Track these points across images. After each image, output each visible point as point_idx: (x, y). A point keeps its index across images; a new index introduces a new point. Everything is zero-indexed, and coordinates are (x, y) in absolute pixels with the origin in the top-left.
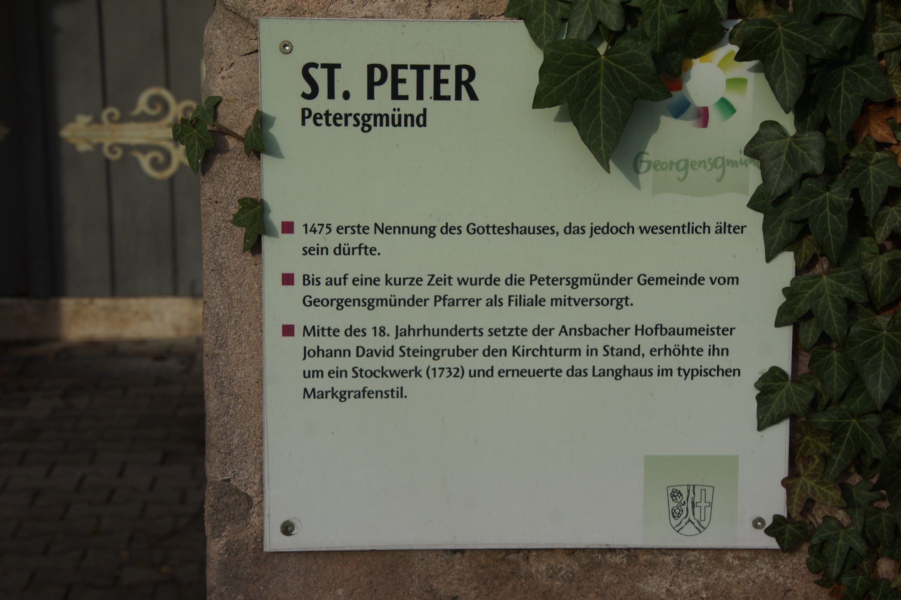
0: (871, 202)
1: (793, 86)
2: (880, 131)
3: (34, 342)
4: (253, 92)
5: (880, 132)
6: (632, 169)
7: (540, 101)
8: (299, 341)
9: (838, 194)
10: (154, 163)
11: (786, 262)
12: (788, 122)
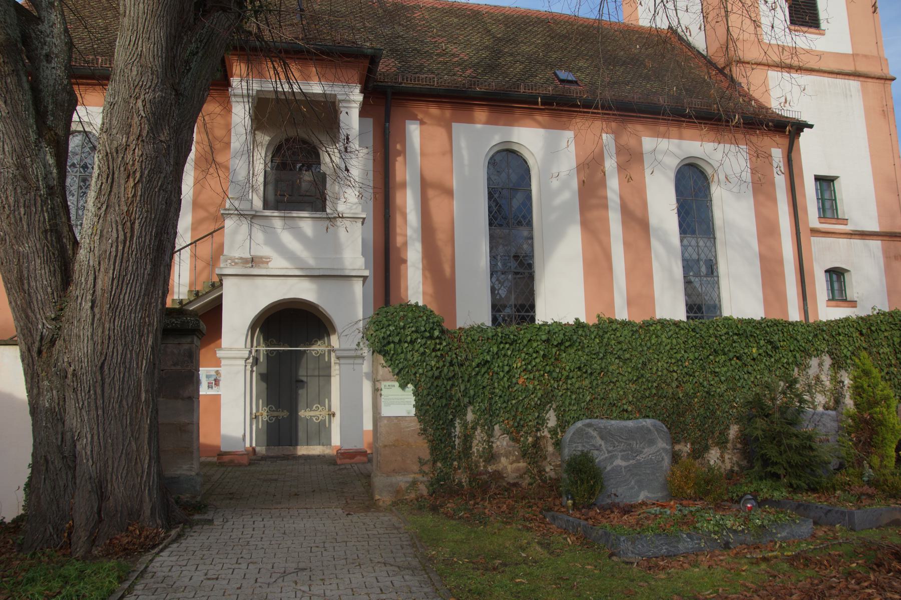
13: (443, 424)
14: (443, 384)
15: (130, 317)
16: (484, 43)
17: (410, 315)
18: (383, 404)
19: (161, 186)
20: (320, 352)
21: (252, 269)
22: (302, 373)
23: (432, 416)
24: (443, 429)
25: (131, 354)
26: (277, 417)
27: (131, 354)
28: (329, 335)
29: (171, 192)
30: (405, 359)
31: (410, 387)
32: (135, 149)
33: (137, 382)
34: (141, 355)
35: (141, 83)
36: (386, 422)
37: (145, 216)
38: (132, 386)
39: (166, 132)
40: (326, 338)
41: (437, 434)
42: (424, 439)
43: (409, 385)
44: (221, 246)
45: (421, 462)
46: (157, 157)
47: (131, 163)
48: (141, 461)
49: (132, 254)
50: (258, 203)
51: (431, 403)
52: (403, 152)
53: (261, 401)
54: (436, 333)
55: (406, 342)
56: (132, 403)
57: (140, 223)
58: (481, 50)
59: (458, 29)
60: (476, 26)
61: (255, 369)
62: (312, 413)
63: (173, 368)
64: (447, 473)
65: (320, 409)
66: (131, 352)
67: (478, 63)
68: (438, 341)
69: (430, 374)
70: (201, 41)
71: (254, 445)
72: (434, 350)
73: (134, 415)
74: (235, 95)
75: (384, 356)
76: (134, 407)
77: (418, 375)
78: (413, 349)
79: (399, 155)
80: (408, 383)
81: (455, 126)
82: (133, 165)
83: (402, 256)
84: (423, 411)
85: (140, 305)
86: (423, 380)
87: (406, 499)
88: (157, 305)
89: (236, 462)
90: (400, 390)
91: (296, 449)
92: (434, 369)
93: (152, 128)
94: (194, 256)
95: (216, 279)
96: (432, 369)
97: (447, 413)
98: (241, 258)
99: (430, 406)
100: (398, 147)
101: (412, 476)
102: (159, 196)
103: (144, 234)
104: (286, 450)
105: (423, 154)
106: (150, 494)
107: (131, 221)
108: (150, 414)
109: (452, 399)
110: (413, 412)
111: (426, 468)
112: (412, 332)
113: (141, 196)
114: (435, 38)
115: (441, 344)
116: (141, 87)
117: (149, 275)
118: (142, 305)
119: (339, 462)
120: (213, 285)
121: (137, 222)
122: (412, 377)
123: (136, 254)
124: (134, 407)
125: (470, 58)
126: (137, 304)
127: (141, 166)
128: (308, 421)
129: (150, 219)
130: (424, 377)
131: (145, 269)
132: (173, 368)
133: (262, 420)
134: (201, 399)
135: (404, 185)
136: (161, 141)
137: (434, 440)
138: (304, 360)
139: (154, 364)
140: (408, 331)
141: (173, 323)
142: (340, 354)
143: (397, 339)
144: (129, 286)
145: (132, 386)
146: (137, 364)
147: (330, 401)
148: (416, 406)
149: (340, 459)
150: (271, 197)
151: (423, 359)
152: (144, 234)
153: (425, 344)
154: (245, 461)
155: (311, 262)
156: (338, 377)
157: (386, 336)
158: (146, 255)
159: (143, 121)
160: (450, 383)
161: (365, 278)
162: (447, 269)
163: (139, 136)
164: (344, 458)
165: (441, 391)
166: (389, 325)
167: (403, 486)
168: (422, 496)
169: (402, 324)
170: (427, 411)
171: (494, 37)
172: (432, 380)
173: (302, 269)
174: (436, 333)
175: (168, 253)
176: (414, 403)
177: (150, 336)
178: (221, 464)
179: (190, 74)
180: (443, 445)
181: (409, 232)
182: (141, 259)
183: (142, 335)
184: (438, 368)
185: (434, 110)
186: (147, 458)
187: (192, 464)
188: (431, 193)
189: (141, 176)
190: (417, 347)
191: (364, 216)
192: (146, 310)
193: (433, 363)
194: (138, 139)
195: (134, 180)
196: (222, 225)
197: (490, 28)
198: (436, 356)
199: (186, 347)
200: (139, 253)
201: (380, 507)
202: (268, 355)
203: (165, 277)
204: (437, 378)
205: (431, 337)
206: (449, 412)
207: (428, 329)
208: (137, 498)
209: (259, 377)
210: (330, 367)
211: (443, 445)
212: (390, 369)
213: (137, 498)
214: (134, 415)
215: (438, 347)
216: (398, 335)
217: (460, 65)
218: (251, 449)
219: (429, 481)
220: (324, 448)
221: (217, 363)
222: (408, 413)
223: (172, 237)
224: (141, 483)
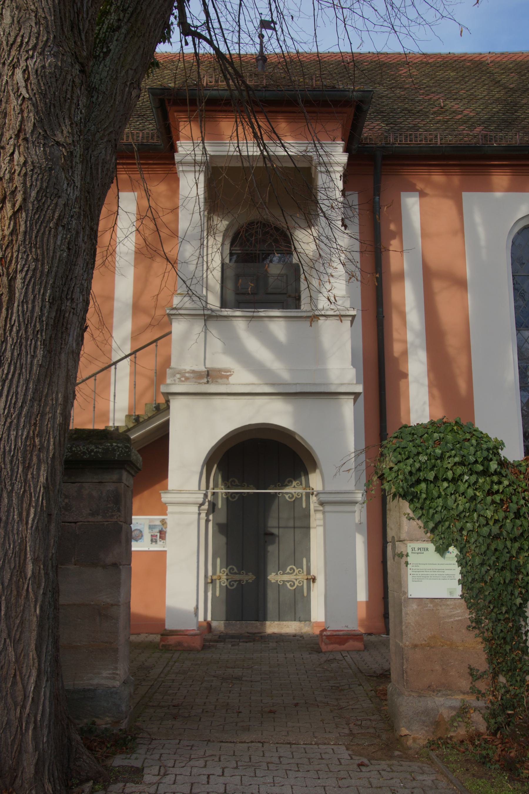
0: (468, 561)
1: (459, 550)
2: (125, 27)
3: (261, 633)
4: (407, 550)
5: (468, 555)
6: (444, 558)
7: (435, 551)
8: (411, 575)
9: (464, 561)
10: (291, 585)
11: (460, 568)
12: (459, 554)
13: (506, 612)
14: (506, 547)
15: (9, 435)
16: (493, 96)
17: (449, 437)
18: (410, 578)
19: (60, 219)
20: (295, 495)
21: (207, 385)
22: (272, 523)
23: (489, 598)
24: (507, 620)
25: (10, 497)
26: (240, 581)
27: (10, 497)
28: (306, 474)
29: (77, 233)
30: (445, 507)
31: (453, 551)
32: (12, 154)
33: (20, 545)
34: (26, 499)
35: (19, 40)
36: (415, 606)
37: (32, 267)
38: (10, 552)
39: (66, 130)
40: (303, 478)
41: (499, 629)
42: (476, 636)
43: (451, 549)
44: (167, 362)
45: (472, 671)
46: (51, 169)
47: (7, 176)
48: (22, 680)
49: (11, 331)
50: (214, 301)
51: (488, 579)
52: (398, 234)
53: (218, 561)
54: (494, 466)
55: (446, 479)
56: (10, 580)
57: (25, 278)
58: (491, 104)
59: (457, 83)
60: (480, 78)
62: (286, 577)
63: (91, 519)
64: (516, 695)
65: (296, 571)
66: (10, 494)
67: (489, 119)
68: (495, 478)
69: (485, 531)
70: (124, 11)
71: (209, 619)
72: (490, 493)
73: (13, 600)
74: (181, 163)
75: (411, 501)
76: (13, 586)
77: (465, 533)
78: (456, 491)
79: (394, 238)
80: (449, 545)
81: (466, 196)
82: (11, 180)
83: (402, 368)
84: (475, 591)
85: (26, 416)
86: (473, 540)
87: (451, 738)
88: (54, 417)
89: (186, 645)
90: (437, 555)
91: (263, 625)
92: (491, 523)
93: (41, 121)
94: (134, 373)
95: (161, 400)
96: (487, 524)
97: (512, 594)
98: (193, 372)
99: (486, 582)
100: (392, 227)
101: (461, 697)
102: (56, 236)
103: (31, 297)
104: (250, 627)
105: (424, 235)
106: (35, 738)
107: (8, 274)
108: (40, 598)
109: (519, 572)
110: (458, 591)
111: (482, 686)
112: (455, 464)
113: (25, 233)
114: (428, 95)
115: (500, 483)
116: (21, 46)
117: (41, 366)
118: (29, 416)
119: (324, 647)
120: (158, 408)
121: (19, 276)
122: (456, 536)
123: (18, 332)
124: (13, 586)
125: (477, 114)
126: (20, 414)
127: (25, 183)
128: (279, 587)
129: (42, 272)
130: (475, 535)
131: (33, 357)
132: (91, 519)
133: (220, 585)
134: (134, 564)
135: (401, 276)
136: (58, 143)
137: (493, 639)
138: (275, 507)
139: (50, 515)
140: (448, 463)
141: (92, 451)
142: (323, 498)
143: (431, 476)
144: (7, 382)
145: (10, 552)
146: (20, 514)
147: (308, 561)
148: (462, 582)
149: (326, 644)
150: (230, 296)
151: (472, 507)
152: (31, 297)
153: (476, 483)
154: (197, 643)
155: (286, 376)
156: (320, 530)
157: (414, 471)
158: (36, 333)
159: (25, 106)
160: (517, 545)
161: (356, 395)
162: (462, 384)
163: (19, 131)
164: (332, 643)
165: (503, 559)
166: (418, 454)
167: (447, 714)
168: (479, 735)
169: (438, 451)
170: (481, 591)
171: (505, 88)
172: (489, 541)
173: (273, 385)
174: (494, 466)
175: (74, 333)
176: (460, 577)
177: (43, 467)
178: (166, 648)
179: (108, 59)
180: (508, 648)
181: (410, 337)
182: (27, 339)
183: (29, 467)
184: (496, 521)
185: (438, 178)
186: (34, 673)
187: (116, 669)
188: (437, 285)
189: (24, 200)
190: (462, 487)
191: (353, 312)
192: (35, 424)
193: (489, 514)
194: (17, 136)
195: (14, 205)
196: (166, 331)
197: (499, 79)
198: (493, 502)
199: (111, 487)
200: (23, 328)
201: (409, 748)
202: (229, 499)
203: (68, 370)
204: (497, 537)
205: (485, 473)
206: (516, 592)
207: (480, 460)
208: (12, 744)
210: (308, 516)
211: (508, 648)
212: (420, 523)
213: (12, 744)
214: (13, 600)
215: (496, 487)
216: (432, 469)
217: (465, 123)
218: (205, 624)
219: (487, 708)
220: (302, 624)
221: (162, 509)
222: (451, 593)
223: (80, 306)
224: (21, 718)
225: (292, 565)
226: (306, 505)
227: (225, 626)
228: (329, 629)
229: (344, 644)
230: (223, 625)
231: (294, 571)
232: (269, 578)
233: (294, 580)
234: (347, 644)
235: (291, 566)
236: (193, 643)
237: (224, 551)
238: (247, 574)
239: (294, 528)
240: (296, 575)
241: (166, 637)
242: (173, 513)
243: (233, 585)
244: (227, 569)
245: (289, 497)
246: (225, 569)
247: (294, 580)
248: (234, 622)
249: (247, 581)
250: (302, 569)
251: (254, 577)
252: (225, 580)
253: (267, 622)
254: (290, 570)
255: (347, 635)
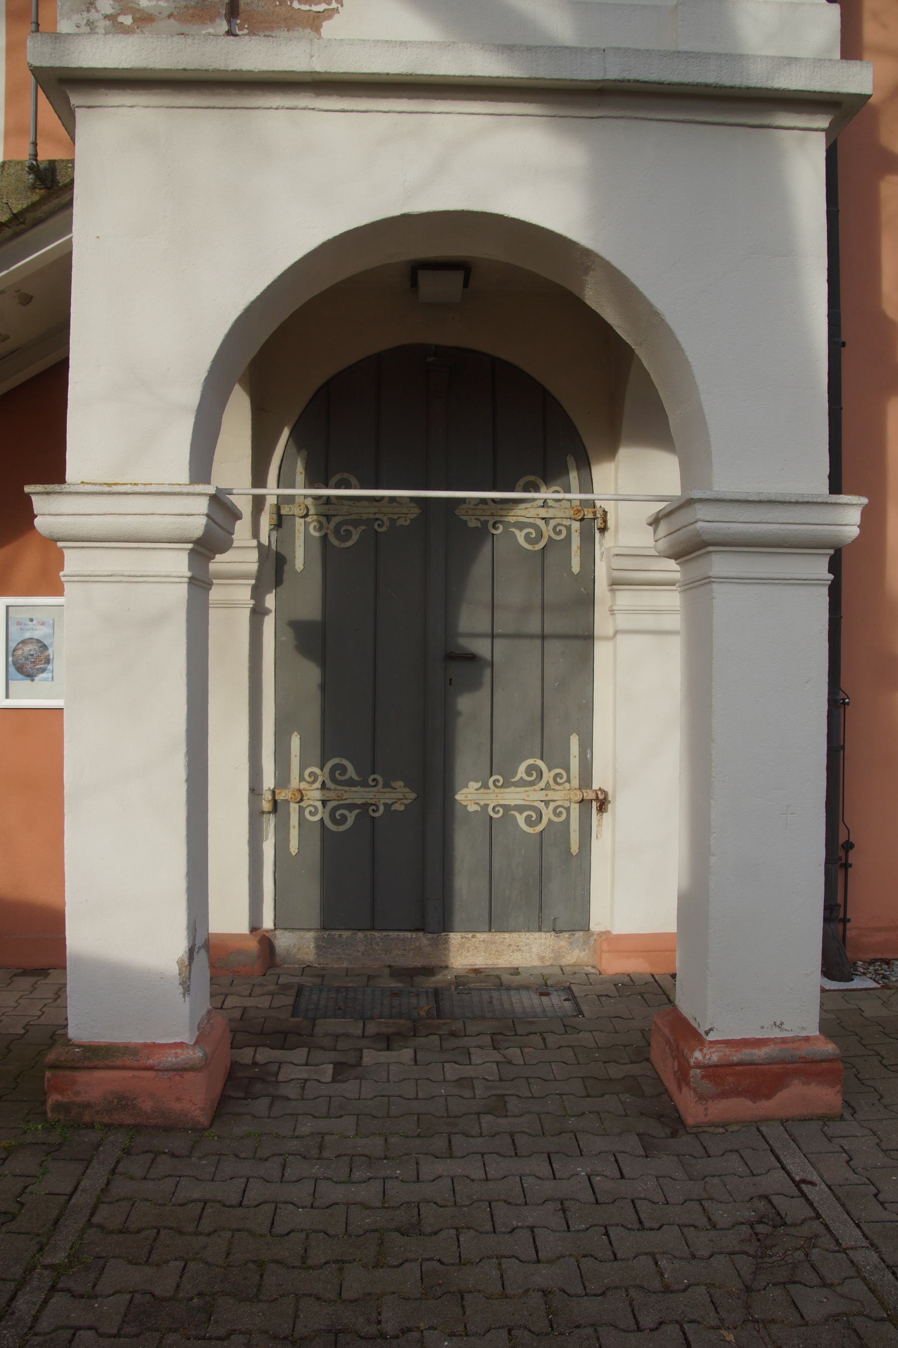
3: (429, 971)
10: (529, 822)
26: (365, 806)
28: (585, 464)
40: (573, 476)
53: (295, 742)
61: (270, 601)
62: (513, 796)
65: (548, 776)
71: (268, 923)
91: (441, 946)
138: (480, 569)
147: (587, 745)
149: (702, 1098)
164: (724, 1095)
173: (508, 49)
209: (289, 637)
210: (588, 601)
218: (253, 945)
220: (563, 941)
225: (532, 756)
226: (582, 566)
227: (318, 947)
228: (711, 1037)
229: (768, 1097)
230: (312, 945)
231: (540, 775)
232: (458, 797)
233: (541, 806)
234: (781, 1097)
235: (530, 761)
236: (178, 1100)
237: (312, 713)
238: (387, 785)
239: (543, 637)
240: (547, 787)
241: (68, 1073)
242: (85, 579)
243: (344, 819)
244: (322, 770)
245: (527, 537)
246: (317, 770)
247: (541, 806)
248: (346, 934)
249: (387, 806)
250: (568, 771)
251: (413, 796)
252: (319, 804)
253: (452, 935)
254: (528, 772)
255: (783, 1061)
